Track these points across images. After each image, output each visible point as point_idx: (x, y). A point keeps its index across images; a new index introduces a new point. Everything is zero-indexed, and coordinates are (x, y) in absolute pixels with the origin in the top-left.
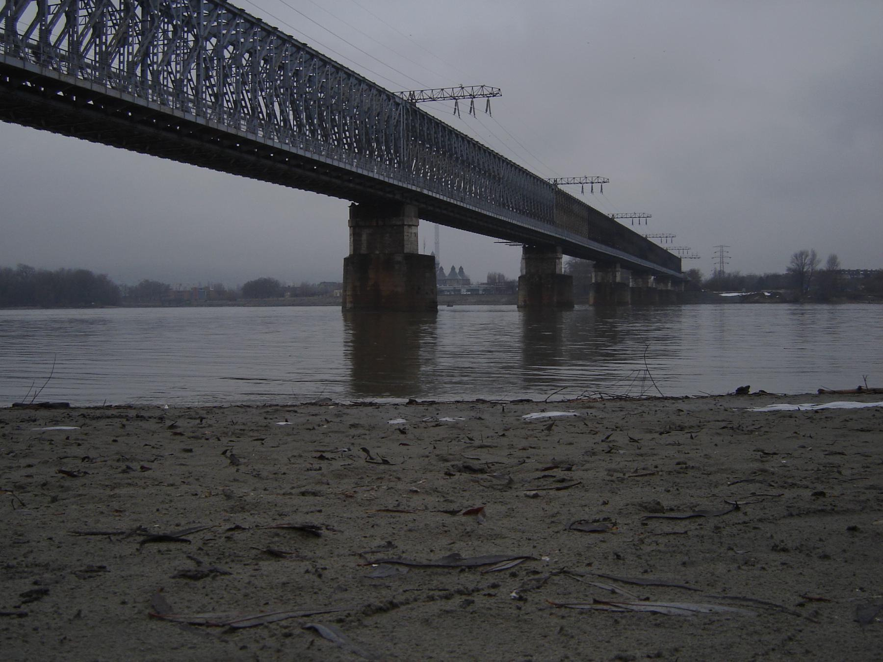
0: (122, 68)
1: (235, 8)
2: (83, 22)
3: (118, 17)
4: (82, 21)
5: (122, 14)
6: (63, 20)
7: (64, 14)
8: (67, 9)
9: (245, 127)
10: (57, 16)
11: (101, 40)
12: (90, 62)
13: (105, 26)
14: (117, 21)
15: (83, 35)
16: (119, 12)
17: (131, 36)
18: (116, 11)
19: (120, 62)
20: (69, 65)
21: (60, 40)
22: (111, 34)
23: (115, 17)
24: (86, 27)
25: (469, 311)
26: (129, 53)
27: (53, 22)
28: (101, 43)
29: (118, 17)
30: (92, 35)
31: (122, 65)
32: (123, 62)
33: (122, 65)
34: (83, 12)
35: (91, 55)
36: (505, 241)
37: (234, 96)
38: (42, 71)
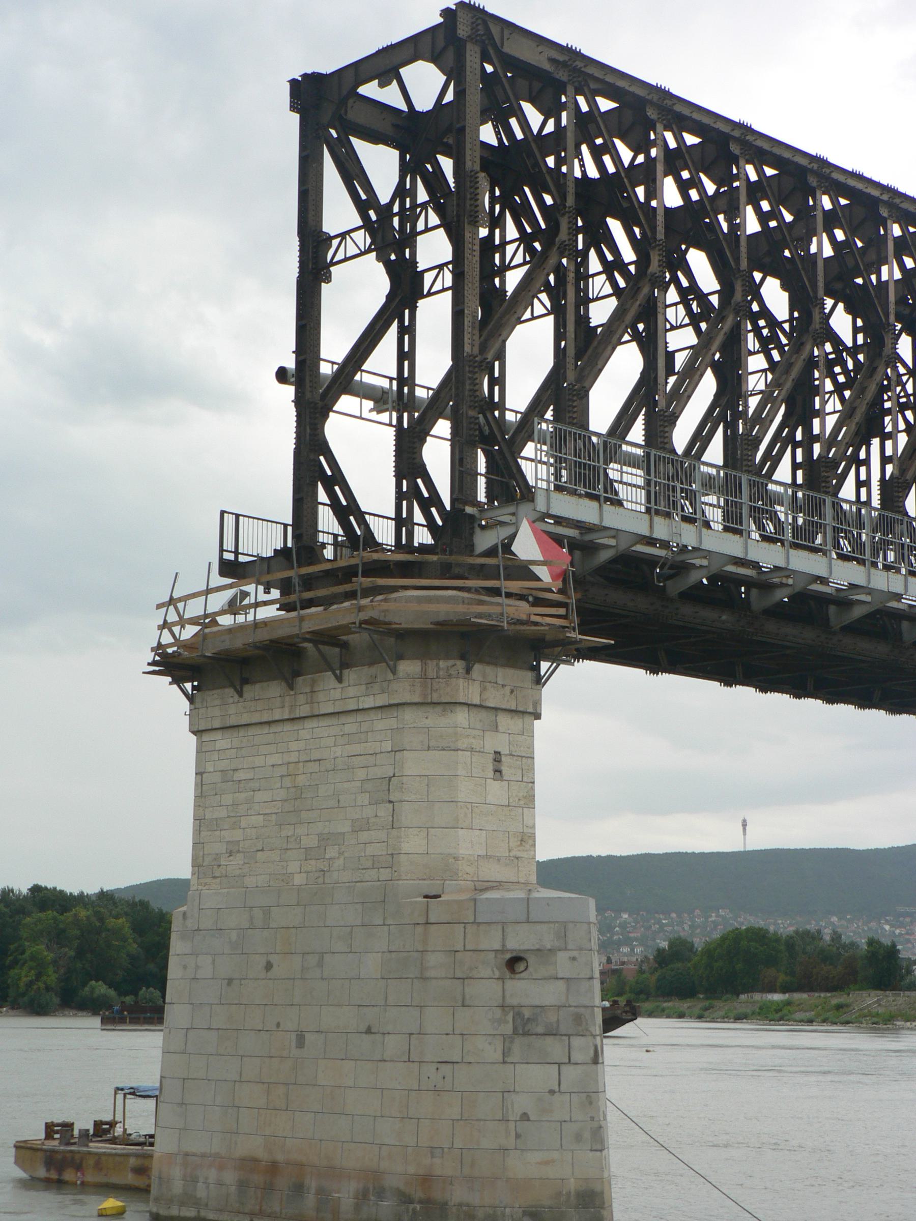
0: (863, 498)
1: (870, 181)
2: (761, 386)
3: (850, 365)
4: (756, 382)
5: (861, 357)
6: (708, 385)
7: (709, 371)
8: (717, 356)
9: (641, 495)
10: (691, 374)
11: (808, 429)
12: (780, 489)
13: (817, 391)
14: (909, 399)
15: (760, 420)
16: (854, 350)
17: (889, 412)
18: (846, 348)
19: (859, 484)
20: (400, 419)
21: (701, 438)
22: (835, 412)
23: (904, 389)
24: (767, 396)
25: (703, 1046)
26: (885, 460)
27: (681, 397)
28: (810, 439)
29: (850, 365)
30: (785, 416)
31: (863, 491)
32: (867, 483)
33: (863, 491)
34: (757, 362)
35: (783, 472)
36: (394, 626)
37: (889, 468)
38: (651, 527)
